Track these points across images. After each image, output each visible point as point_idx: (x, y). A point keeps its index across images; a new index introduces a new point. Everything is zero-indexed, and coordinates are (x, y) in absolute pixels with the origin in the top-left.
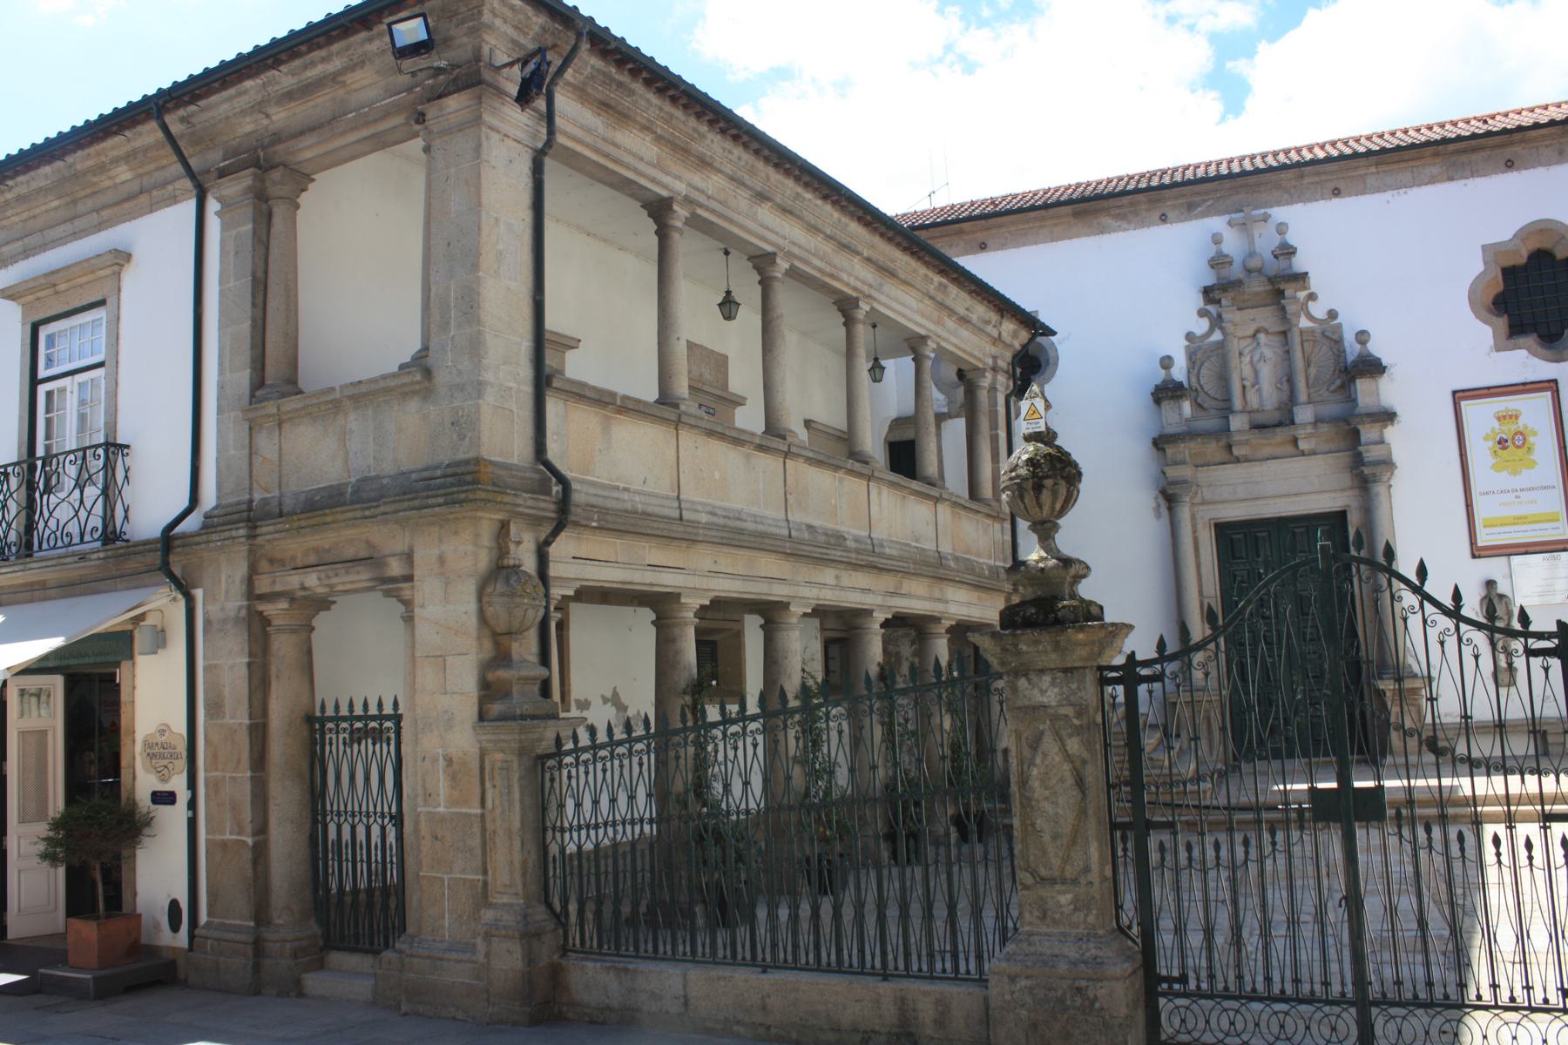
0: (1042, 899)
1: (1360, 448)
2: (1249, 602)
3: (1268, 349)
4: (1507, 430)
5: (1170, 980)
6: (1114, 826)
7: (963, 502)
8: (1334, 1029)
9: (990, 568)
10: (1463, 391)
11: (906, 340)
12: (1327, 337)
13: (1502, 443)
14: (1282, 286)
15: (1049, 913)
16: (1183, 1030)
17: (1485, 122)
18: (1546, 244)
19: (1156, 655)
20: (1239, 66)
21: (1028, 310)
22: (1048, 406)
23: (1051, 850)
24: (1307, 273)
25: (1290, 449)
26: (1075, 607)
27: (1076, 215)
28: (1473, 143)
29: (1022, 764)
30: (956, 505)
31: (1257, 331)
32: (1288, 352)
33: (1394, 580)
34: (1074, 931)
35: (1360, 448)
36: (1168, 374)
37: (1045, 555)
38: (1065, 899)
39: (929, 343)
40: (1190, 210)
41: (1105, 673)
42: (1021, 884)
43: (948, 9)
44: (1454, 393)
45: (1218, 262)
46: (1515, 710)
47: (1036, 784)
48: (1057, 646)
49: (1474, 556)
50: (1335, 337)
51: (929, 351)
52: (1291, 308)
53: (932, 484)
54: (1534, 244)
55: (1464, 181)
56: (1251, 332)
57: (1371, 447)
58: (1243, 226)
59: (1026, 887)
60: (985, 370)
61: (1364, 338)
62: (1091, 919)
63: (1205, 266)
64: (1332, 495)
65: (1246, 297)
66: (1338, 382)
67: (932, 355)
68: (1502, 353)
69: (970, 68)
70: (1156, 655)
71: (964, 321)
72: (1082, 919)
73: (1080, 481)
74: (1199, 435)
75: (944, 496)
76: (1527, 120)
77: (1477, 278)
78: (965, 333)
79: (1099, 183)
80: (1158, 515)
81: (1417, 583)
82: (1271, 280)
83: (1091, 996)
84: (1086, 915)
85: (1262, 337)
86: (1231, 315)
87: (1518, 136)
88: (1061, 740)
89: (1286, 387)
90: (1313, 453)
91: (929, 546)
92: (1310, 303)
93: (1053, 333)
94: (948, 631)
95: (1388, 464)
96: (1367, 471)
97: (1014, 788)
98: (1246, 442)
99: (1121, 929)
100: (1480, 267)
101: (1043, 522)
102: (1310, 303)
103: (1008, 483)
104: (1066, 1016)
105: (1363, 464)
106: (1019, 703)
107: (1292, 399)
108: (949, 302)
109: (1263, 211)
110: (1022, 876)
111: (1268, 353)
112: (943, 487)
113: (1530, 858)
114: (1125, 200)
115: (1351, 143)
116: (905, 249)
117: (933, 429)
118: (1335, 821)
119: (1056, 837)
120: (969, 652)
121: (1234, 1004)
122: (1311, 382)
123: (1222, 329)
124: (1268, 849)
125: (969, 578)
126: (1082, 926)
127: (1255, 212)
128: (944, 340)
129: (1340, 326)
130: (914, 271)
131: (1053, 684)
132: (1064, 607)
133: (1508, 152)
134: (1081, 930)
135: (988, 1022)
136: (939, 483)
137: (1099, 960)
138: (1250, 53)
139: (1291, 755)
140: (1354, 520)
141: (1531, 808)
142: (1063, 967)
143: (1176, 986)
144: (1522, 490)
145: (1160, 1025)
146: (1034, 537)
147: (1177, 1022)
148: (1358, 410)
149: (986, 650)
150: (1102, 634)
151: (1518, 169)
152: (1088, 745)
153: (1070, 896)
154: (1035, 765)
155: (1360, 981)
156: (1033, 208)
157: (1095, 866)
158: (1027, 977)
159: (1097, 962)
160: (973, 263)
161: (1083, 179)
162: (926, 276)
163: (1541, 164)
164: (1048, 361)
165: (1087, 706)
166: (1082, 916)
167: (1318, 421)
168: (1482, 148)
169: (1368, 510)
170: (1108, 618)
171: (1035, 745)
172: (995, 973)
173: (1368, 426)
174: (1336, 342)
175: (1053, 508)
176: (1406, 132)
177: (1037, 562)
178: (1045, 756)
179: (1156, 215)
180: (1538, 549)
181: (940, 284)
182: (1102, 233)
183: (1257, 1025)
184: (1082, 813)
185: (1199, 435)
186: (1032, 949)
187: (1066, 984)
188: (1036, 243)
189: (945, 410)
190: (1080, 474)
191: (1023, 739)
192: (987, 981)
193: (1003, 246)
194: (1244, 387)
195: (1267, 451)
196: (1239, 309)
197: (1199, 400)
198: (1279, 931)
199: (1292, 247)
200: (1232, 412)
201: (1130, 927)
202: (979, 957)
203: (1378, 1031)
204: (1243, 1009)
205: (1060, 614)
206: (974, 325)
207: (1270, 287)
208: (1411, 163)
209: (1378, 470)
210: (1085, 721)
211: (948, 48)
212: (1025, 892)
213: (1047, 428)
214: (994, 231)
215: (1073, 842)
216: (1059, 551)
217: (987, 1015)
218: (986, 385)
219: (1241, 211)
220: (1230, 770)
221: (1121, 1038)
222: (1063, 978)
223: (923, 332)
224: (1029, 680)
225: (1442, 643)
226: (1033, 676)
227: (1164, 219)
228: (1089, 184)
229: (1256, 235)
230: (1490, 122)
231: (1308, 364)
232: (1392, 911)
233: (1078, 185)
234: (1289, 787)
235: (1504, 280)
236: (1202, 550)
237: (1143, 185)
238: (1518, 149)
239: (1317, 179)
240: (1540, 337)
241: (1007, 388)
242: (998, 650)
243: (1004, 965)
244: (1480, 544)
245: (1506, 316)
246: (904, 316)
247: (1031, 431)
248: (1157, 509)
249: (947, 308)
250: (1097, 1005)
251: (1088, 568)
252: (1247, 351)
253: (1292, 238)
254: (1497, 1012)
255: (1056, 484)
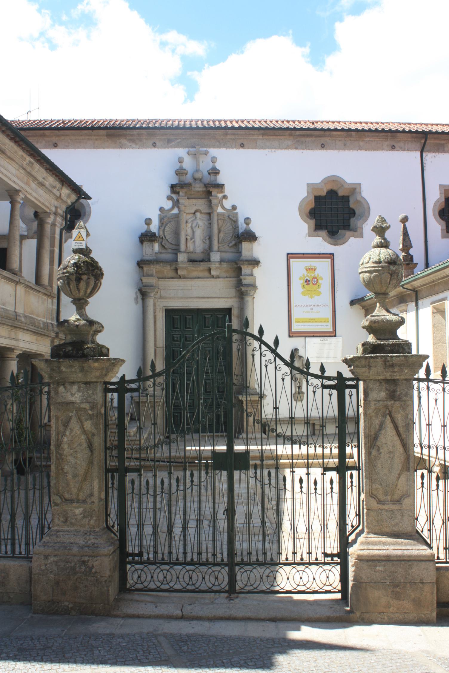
0: (65, 511)
1: (241, 277)
2: (188, 352)
3: (201, 221)
4: (311, 275)
5: (133, 555)
6: (107, 471)
7: (31, 285)
8: (216, 578)
9: (44, 323)
10: (292, 254)
11: (7, 191)
12: (230, 219)
13: (307, 281)
14: (211, 190)
15: (69, 519)
16: (139, 582)
17: (313, 124)
18: (335, 188)
19: (136, 378)
20: (194, 75)
21: (77, 183)
22: (88, 235)
23: (72, 484)
24: (224, 185)
25: (207, 274)
26: (94, 348)
27: (108, 136)
28: (308, 132)
29: (58, 435)
30: (27, 286)
31: (196, 211)
32: (210, 224)
33: (262, 345)
34: (82, 529)
35: (241, 277)
36: (149, 228)
37: (79, 317)
38: (78, 511)
39: (20, 194)
40: (169, 143)
41: (108, 386)
42: (54, 503)
43: (43, 11)
44: (288, 254)
45: (180, 172)
46: (299, 413)
47: (65, 446)
48: (82, 370)
49: (290, 336)
50: (234, 219)
51: (20, 198)
52: (214, 201)
53: (15, 273)
54: (329, 187)
55: (302, 151)
56: (193, 211)
57: (247, 277)
58: (195, 156)
59: (56, 504)
60: (50, 213)
61: (248, 221)
62: (92, 522)
63: (173, 173)
64: (226, 300)
65: (192, 193)
66: (234, 243)
67: (22, 202)
68: (311, 237)
69: (53, 47)
70: (136, 378)
71: (41, 185)
72: (87, 523)
73: (102, 278)
74: (161, 262)
75: (21, 281)
76: (332, 126)
77: (303, 199)
78: (41, 191)
79: (122, 121)
80: (137, 302)
81: (274, 348)
82: (206, 186)
83: (91, 566)
84: (90, 520)
85: (198, 214)
86: (183, 201)
87: (327, 133)
88: (81, 422)
89: (207, 242)
90: (218, 277)
91: (11, 308)
92: (224, 200)
93: (90, 198)
94: (18, 357)
95: (254, 286)
96: (243, 289)
97: (53, 447)
98: (185, 268)
99: (108, 527)
100: (305, 194)
101: (80, 299)
102: (224, 200)
103: (61, 275)
104: (76, 577)
105: (242, 286)
106: (59, 401)
107: (209, 250)
108: (33, 173)
109: (205, 149)
110: (56, 499)
111: (201, 223)
112: (21, 276)
113: (316, 489)
114: (135, 132)
115: (251, 122)
116: (11, 139)
117: (18, 243)
118: (224, 470)
119: (75, 476)
120: (29, 369)
121: (167, 567)
122: (220, 241)
123: (178, 207)
124: (189, 484)
125: (32, 328)
126: (87, 526)
127: (201, 149)
128: (29, 194)
129: (237, 214)
130: (16, 152)
131: (79, 390)
132: (88, 348)
133: (323, 140)
134: (87, 528)
135: (31, 581)
136: (18, 273)
137: (96, 545)
138: (200, 69)
139: (204, 431)
140: (235, 312)
141: (302, 461)
142: (75, 549)
143: (136, 558)
144: (314, 306)
145: (126, 579)
146: (74, 307)
147: (135, 576)
148: (242, 258)
149: (41, 369)
150: (108, 364)
151: (326, 149)
152: (96, 425)
153: (81, 509)
154: (65, 435)
155: (231, 553)
156: (85, 128)
157: (96, 493)
158: (55, 556)
159: (95, 546)
160: (51, 154)
161: (114, 118)
162: (22, 156)
163: (336, 149)
164: (85, 213)
165: (97, 404)
166: (88, 521)
167: (222, 261)
168: (311, 136)
169: (242, 309)
170: (111, 356)
171: (66, 425)
172: (36, 554)
173: (246, 266)
174: (235, 222)
175: (86, 292)
176: (277, 122)
177: (75, 321)
178: (72, 430)
179: (150, 143)
180: (318, 335)
181: (30, 162)
182: (121, 148)
183: (178, 578)
184: (91, 463)
185: (161, 262)
186: (59, 540)
187: (76, 559)
188: (85, 148)
189: (26, 233)
190: (102, 274)
191: (60, 422)
192: (31, 558)
193: (66, 147)
194: (187, 239)
195: (195, 274)
196: (188, 198)
197: (163, 243)
198: (192, 524)
199: (218, 170)
200: (180, 252)
201: (113, 526)
202: (27, 544)
203: (238, 578)
204: (146, 569)
205: (85, 351)
206: (46, 188)
207: (205, 189)
208: (279, 137)
209: (249, 289)
210: (95, 412)
211: (42, 34)
212: (56, 507)
213: (87, 247)
214: (63, 138)
215: (85, 479)
216: (87, 316)
217: (31, 577)
218: (50, 222)
219: (194, 147)
220: (168, 440)
221: (106, 588)
222: (75, 556)
223: (17, 188)
224: (65, 387)
225: (283, 379)
226: (67, 385)
227: (154, 145)
228: (116, 121)
229: (201, 162)
230: (315, 124)
231: (220, 232)
232: (249, 516)
233: (111, 121)
234: (202, 448)
235: (315, 202)
236: (158, 322)
237: (145, 125)
238: (327, 139)
239: (233, 137)
240: (328, 232)
241: (62, 225)
242: (49, 369)
243: (42, 549)
244: (293, 330)
245: (314, 220)
246: (7, 177)
247: (77, 247)
248: (136, 299)
249: (32, 176)
250: (93, 570)
251: (103, 327)
252: (190, 221)
253: (218, 166)
254: (294, 566)
255: (89, 278)
